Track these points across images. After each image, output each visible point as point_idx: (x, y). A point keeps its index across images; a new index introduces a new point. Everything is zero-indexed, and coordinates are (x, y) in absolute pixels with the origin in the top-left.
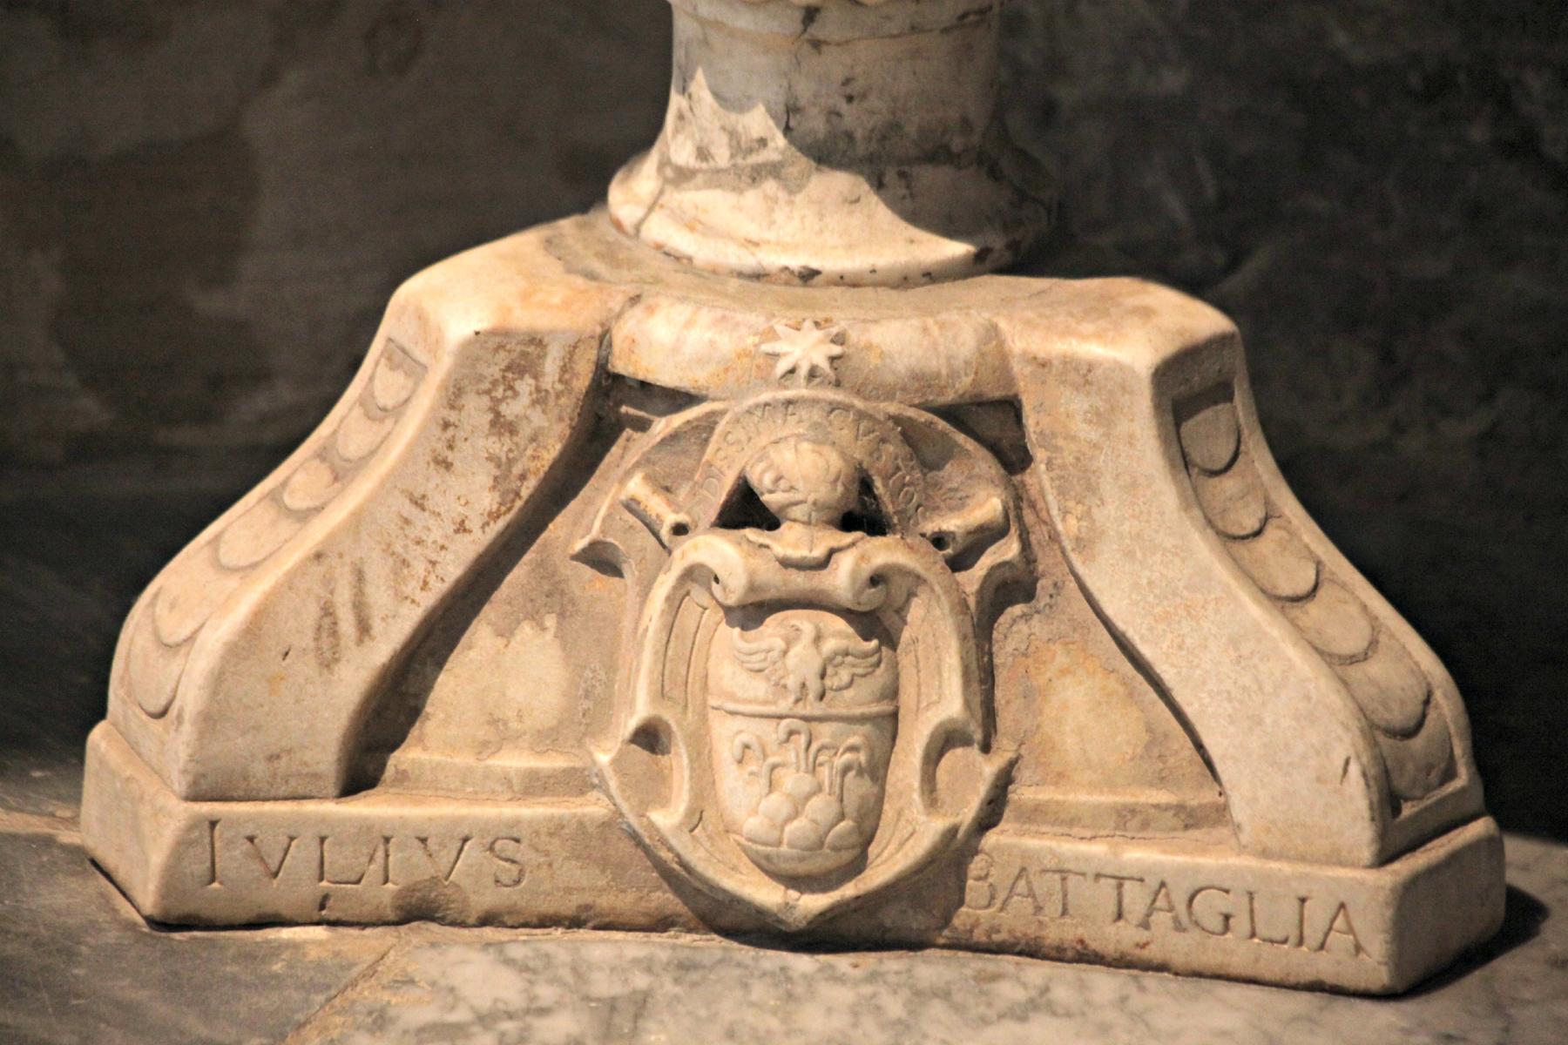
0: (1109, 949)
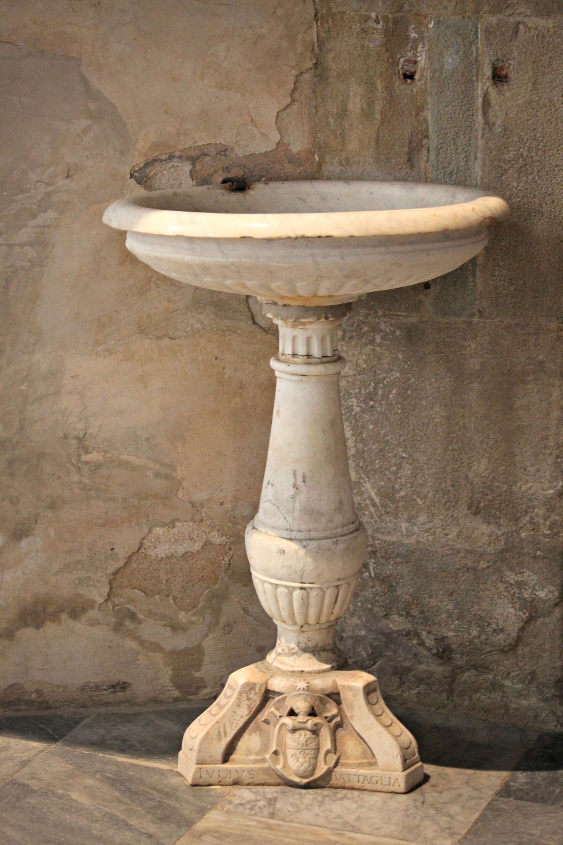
0: (357, 787)
